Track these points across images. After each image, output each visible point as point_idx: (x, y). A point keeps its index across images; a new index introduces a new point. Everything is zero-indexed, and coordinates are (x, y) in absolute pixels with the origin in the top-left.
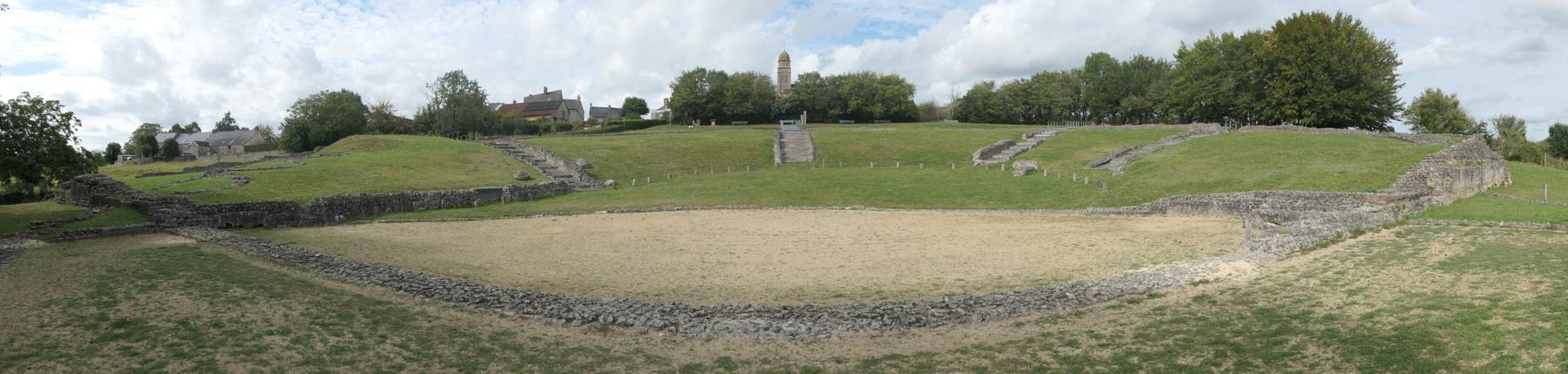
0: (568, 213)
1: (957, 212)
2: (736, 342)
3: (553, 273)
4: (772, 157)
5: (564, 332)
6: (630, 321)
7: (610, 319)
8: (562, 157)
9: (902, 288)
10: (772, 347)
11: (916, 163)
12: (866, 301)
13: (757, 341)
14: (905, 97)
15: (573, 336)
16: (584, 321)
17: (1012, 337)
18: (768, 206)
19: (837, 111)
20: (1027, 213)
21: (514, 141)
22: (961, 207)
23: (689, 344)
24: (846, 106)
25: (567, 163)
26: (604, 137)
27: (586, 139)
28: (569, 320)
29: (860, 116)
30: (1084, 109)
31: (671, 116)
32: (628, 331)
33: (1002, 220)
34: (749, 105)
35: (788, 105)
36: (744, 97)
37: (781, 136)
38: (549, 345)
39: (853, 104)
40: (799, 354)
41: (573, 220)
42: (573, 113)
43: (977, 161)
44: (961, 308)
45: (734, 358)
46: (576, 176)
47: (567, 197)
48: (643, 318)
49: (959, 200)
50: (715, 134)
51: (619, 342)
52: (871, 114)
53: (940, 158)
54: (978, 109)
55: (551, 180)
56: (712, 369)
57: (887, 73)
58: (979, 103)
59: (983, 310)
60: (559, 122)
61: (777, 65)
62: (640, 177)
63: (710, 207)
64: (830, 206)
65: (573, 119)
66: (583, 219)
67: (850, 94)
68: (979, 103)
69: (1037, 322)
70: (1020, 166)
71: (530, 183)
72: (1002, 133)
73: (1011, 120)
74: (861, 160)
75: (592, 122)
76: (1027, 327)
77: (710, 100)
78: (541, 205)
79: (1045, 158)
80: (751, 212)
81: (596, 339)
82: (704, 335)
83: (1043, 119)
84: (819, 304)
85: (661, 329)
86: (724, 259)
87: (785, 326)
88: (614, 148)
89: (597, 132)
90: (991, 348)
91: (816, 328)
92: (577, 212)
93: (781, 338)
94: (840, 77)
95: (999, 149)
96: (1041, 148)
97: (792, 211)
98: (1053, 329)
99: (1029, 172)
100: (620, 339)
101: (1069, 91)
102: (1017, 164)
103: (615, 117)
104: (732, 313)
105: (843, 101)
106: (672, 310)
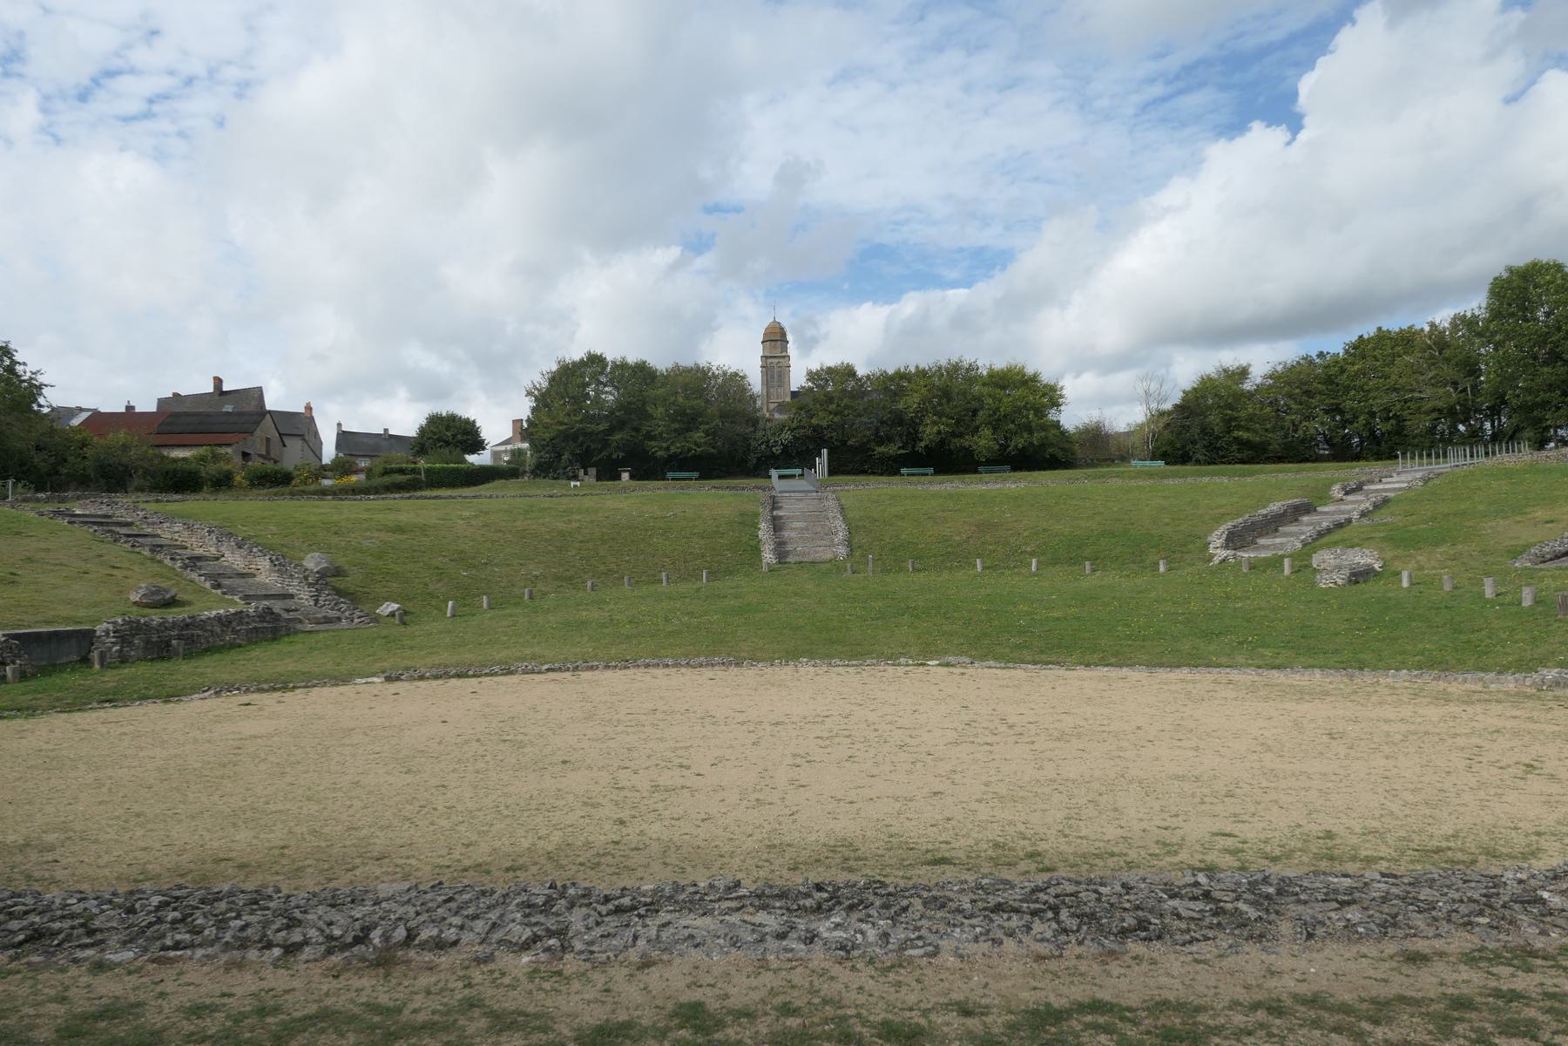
0: (282, 685)
1: (1184, 673)
2: (714, 967)
3: (243, 836)
4: (756, 550)
5: (278, 980)
6: (450, 935)
7: (400, 933)
8: (266, 549)
9: (1085, 847)
10: (798, 976)
11: (1075, 561)
12: (1006, 874)
13: (763, 965)
14: (1040, 412)
15: (303, 985)
16: (333, 945)
17: (1400, 983)
18: (754, 659)
19: (892, 449)
20: (1367, 677)
21: (123, 507)
22: (1195, 660)
23: (599, 978)
24: (914, 437)
25: (279, 565)
26: (374, 503)
27: (327, 507)
28: (291, 949)
29: (949, 459)
30: (1494, 412)
31: (530, 458)
32: (444, 960)
33: (1302, 695)
34: (698, 436)
35: (787, 436)
36: (688, 420)
37: (775, 505)
38: (239, 1018)
39: (930, 431)
40: (866, 993)
41: (297, 702)
42: (294, 446)
43: (1219, 553)
44: (1245, 902)
45: (713, 1005)
46: (304, 596)
47: (282, 646)
48: (479, 925)
49: (1186, 646)
50: (629, 501)
51: (420, 990)
52: (969, 452)
53: (1130, 547)
54: (1211, 430)
55: (237, 605)
56: (662, 1034)
57: (1000, 364)
58: (1214, 419)
59: (1307, 912)
60: (256, 463)
61: (759, 351)
62: (466, 596)
63: (625, 663)
64: (892, 658)
65: (292, 457)
66: (323, 699)
67: (922, 412)
68: (1214, 419)
69: (1470, 959)
70: (1332, 564)
71: (174, 615)
72: (1277, 485)
73: (1297, 452)
74: (954, 556)
75: (341, 467)
76: (1439, 967)
77: (618, 425)
78: (210, 667)
79: (1403, 540)
80: (718, 673)
81: (367, 988)
82: (633, 955)
83: (1384, 444)
84: (895, 879)
85: (526, 946)
86: (666, 779)
87: (823, 927)
88: (399, 529)
89: (355, 491)
90: (1345, 1009)
91: (899, 935)
92: (309, 681)
93: (818, 957)
94: (901, 376)
95: (1272, 524)
96: (1384, 517)
97: (807, 670)
98: (1522, 982)
99: (1360, 576)
100: (425, 980)
101: (1448, 371)
102: (1324, 558)
103: (400, 457)
104: (696, 902)
105: (906, 426)
106: (549, 902)
